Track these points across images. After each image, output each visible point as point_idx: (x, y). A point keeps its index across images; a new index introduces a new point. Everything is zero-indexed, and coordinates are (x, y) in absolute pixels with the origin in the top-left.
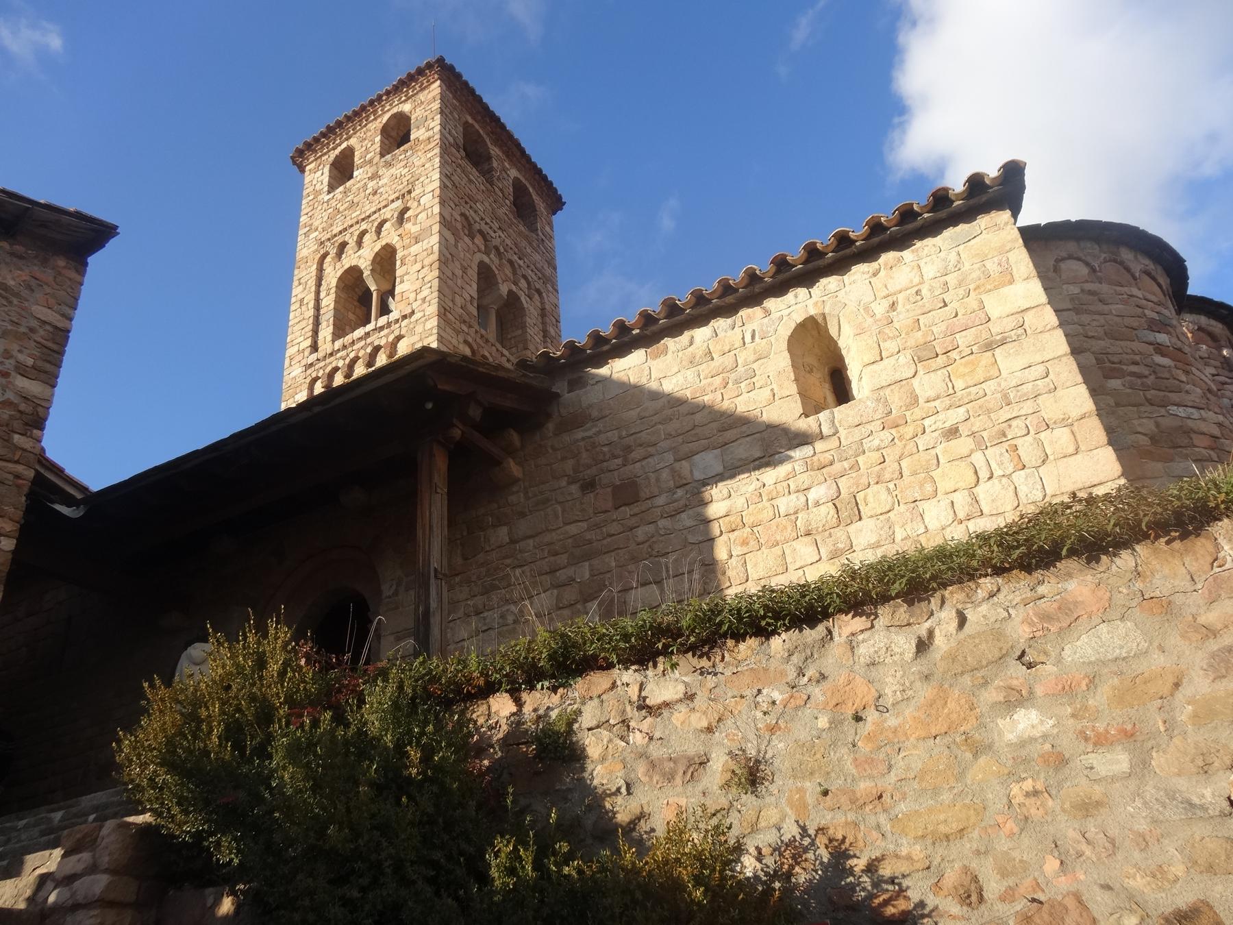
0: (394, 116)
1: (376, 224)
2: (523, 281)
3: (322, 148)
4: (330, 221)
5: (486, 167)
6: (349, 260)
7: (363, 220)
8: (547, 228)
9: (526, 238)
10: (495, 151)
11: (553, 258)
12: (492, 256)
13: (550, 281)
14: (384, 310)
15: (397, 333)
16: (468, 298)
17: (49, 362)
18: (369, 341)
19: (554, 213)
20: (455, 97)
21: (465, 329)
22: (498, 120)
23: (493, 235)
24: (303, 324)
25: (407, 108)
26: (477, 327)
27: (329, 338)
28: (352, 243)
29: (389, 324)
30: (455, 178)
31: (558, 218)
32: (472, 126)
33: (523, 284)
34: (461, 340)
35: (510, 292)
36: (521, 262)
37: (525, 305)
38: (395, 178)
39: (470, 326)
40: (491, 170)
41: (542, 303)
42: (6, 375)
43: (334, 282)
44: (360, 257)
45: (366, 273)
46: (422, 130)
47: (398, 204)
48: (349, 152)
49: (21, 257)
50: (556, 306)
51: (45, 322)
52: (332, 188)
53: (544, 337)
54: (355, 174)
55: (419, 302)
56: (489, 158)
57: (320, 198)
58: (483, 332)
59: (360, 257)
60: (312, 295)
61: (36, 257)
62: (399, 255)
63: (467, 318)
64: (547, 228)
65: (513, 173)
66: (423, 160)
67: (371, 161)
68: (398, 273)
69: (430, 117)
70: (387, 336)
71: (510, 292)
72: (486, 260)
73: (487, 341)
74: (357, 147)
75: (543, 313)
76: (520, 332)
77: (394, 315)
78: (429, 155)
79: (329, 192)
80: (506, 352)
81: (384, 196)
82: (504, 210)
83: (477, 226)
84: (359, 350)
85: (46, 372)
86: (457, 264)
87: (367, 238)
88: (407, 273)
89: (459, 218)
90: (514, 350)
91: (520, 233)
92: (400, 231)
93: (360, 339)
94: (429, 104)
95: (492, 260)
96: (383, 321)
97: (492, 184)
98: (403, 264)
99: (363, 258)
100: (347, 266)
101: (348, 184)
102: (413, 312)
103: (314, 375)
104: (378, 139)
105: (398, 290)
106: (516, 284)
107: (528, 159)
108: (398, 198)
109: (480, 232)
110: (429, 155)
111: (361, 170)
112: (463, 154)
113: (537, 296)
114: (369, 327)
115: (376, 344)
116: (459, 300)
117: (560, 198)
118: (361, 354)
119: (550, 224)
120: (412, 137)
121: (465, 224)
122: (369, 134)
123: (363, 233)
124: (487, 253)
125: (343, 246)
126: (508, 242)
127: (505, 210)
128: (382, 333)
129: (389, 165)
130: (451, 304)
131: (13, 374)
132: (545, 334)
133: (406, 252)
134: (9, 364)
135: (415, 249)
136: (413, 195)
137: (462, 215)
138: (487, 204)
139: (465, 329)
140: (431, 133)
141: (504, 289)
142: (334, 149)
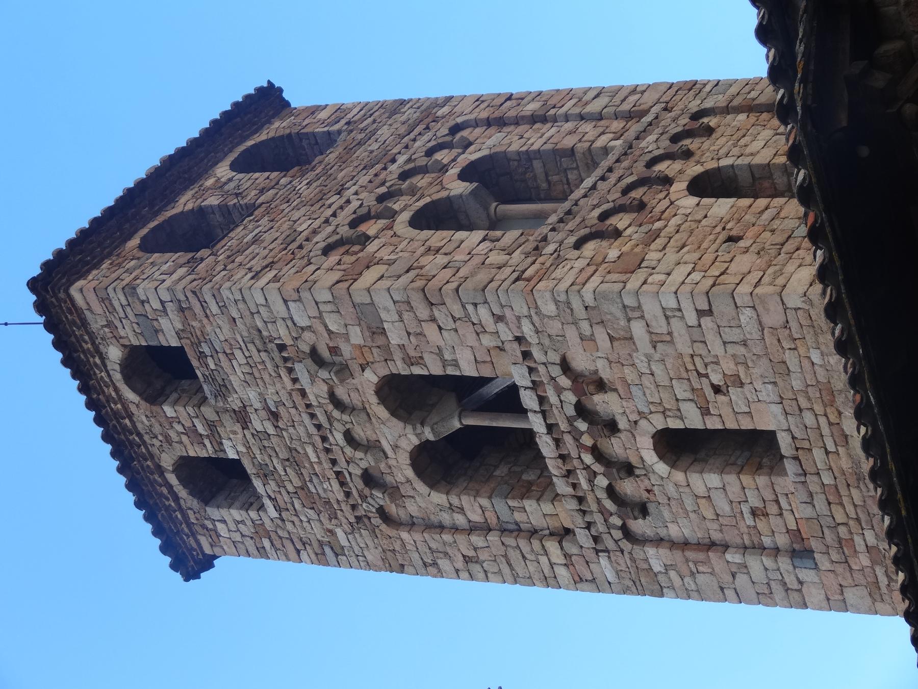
0: (128, 379)
1: (336, 414)
2: (438, 156)
3: (174, 520)
4: (319, 506)
5: (218, 218)
6: (401, 469)
7: (324, 439)
8: (323, 115)
9: (349, 150)
10: (186, 202)
11: (382, 105)
12: (396, 207)
13: (429, 112)
14: (509, 400)
15: (556, 371)
16: (487, 244)
18: (564, 426)
19: (287, 104)
20: (97, 266)
21: (551, 248)
22: (129, 192)
23: (355, 204)
24: (514, 555)
25: (114, 354)
26: (545, 230)
27: (547, 508)
28: (365, 461)
29: (535, 386)
30: (257, 264)
31: (296, 97)
32: (143, 239)
33: (443, 156)
34: (577, 253)
35: (464, 176)
36: (401, 159)
37: (485, 152)
38: (251, 379)
39: (545, 239)
40: (224, 209)
41: (476, 124)
43: (438, 498)
44: (395, 447)
46: (164, 323)
47: (301, 370)
48: (185, 466)
50: (479, 100)
52: (253, 502)
53: (544, 119)
54: (232, 455)
55: (501, 327)
56: (201, 212)
57: (268, 525)
58: (553, 219)
59: (395, 447)
60: (461, 539)
62: (402, 369)
63: (529, 246)
64: (323, 115)
65: (223, 171)
66: (223, 322)
68: (436, 369)
69: (139, 309)
70: (559, 390)
71: (464, 176)
72: (406, 216)
73: (569, 212)
74: (179, 451)
75: (500, 122)
76: (537, 164)
77: (520, 376)
78: (214, 309)
79: (262, 507)
80: (588, 183)
81: (284, 398)
82: (302, 186)
83: (344, 231)
84: (580, 446)
86: (424, 261)
87: (360, 433)
88: (440, 352)
89: (333, 258)
90: (572, 176)
91: (342, 161)
92: (355, 367)
93: (558, 442)
94: (112, 310)
95: (405, 208)
96: (528, 400)
97: (250, 209)
98: (419, 361)
99: (398, 438)
100: (410, 473)
101: (250, 469)
102: (519, 339)
103: (618, 534)
104: (169, 410)
105: (468, 370)
106: (444, 169)
107: (194, 144)
108: (290, 370)
109: (354, 224)
110: (214, 309)
111: (227, 444)
112: (204, 252)
113: (465, 133)
114: (537, 423)
115: (571, 411)
116: (496, 258)
117: (260, 90)
118: (587, 441)
119: (314, 110)
120: (174, 343)
121: (342, 250)
122: (157, 429)
123: (349, 437)
124: (392, 215)
125: (369, 479)
126: (363, 180)
127: (304, 186)
128: (553, 399)
129: (223, 390)
130: (508, 270)
132: (535, 119)
133: (398, 356)
135: (395, 337)
136: (288, 341)
137: (326, 251)
138: (296, 215)
139: (551, 248)
140: (170, 307)
141: (458, 188)
142: (176, 498)
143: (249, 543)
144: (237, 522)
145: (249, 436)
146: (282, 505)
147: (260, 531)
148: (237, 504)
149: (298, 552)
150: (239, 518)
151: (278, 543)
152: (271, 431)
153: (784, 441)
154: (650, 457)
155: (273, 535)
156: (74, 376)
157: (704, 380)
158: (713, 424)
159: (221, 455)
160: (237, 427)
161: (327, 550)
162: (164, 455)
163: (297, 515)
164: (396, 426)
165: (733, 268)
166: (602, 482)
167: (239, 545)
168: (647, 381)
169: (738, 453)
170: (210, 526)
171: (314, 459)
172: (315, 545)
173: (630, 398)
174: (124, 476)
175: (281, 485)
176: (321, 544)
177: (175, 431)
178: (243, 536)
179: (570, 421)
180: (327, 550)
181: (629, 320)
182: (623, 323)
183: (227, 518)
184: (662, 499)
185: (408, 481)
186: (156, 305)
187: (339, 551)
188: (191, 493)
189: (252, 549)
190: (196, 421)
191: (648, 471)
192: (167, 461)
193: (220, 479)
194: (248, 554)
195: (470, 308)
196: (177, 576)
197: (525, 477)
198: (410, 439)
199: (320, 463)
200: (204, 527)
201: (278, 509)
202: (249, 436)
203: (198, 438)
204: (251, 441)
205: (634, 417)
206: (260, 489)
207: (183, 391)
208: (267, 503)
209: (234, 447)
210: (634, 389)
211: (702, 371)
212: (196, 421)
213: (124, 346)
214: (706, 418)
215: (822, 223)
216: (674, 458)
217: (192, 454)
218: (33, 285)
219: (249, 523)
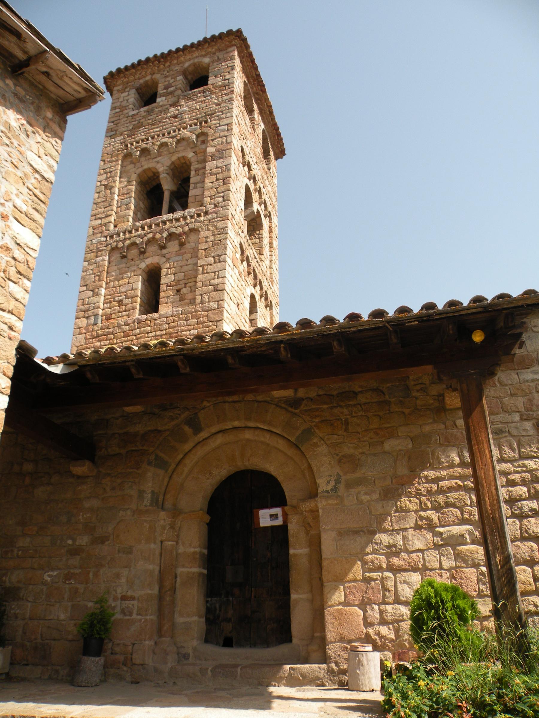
17: (37, 211)
42: (4, 217)
45: (162, 176)
49: (22, 100)
51: (36, 171)
54: (158, 100)
59: (158, 162)
61: (32, 103)
67: (172, 93)
85: (35, 221)
99: (162, 166)
107: (273, 119)
111: (164, 98)
129: (188, 98)
131: (11, 218)
134: (8, 209)
143: (119, 104)
144: (127, 100)
145: (166, 107)
146: (135, 117)
147: (123, 108)
148: (135, 102)
149: (113, 122)
150: (129, 101)
151: (118, 114)
152: (169, 115)
153: (156, 315)
154: (149, 261)
155: (121, 113)
156: (199, 42)
157: (184, 285)
158: (163, 287)
159: (158, 96)
160: (170, 103)
161: (114, 133)
162: (160, 75)
163: (130, 122)
164: (168, 163)
165: (232, 303)
166: (138, 241)
167: (117, 100)
168: (184, 262)
169: (146, 298)
170: (126, 90)
171: (155, 130)
172: (116, 129)
173: (177, 255)
174: (8, 406)
175: (144, 117)
176: (116, 131)
177: (172, 79)
178: (121, 102)
179: (167, 230)
180: (114, 133)
181: (214, 257)
182: (213, 254)
183: (131, 97)
184: (128, 265)
185: (142, 166)
186: (227, 77)
187: (112, 137)
188: (141, 85)
189: (115, 105)
190: (174, 88)
191: (142, 260)
192: (157, 76)
193: (148, 97)
194: (113, 103)
195: (222, 194)
196: (106, 74)
197: (139, 213)
198: (161, 169)
199: (153, 132)
200: (126, 88)
201: (133, 116)
202: (166, 107)
203: (166, 88)
204: (164, 108)
205: (167, 256)
206: (142, 109)
207: (186, 87)
208: (135, 112)
209: (162, 101)
210: (181, 257)
211: (187, 285)
212: (174, 88)
213: (209, 64)
214: (166, 285)
215: (288, 331)
216: (146, 271)
217: (160, 85)
218: (239, 31)
219: (127, 104)
